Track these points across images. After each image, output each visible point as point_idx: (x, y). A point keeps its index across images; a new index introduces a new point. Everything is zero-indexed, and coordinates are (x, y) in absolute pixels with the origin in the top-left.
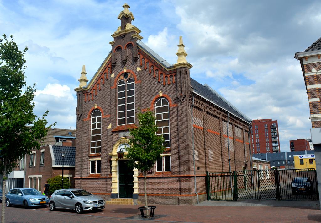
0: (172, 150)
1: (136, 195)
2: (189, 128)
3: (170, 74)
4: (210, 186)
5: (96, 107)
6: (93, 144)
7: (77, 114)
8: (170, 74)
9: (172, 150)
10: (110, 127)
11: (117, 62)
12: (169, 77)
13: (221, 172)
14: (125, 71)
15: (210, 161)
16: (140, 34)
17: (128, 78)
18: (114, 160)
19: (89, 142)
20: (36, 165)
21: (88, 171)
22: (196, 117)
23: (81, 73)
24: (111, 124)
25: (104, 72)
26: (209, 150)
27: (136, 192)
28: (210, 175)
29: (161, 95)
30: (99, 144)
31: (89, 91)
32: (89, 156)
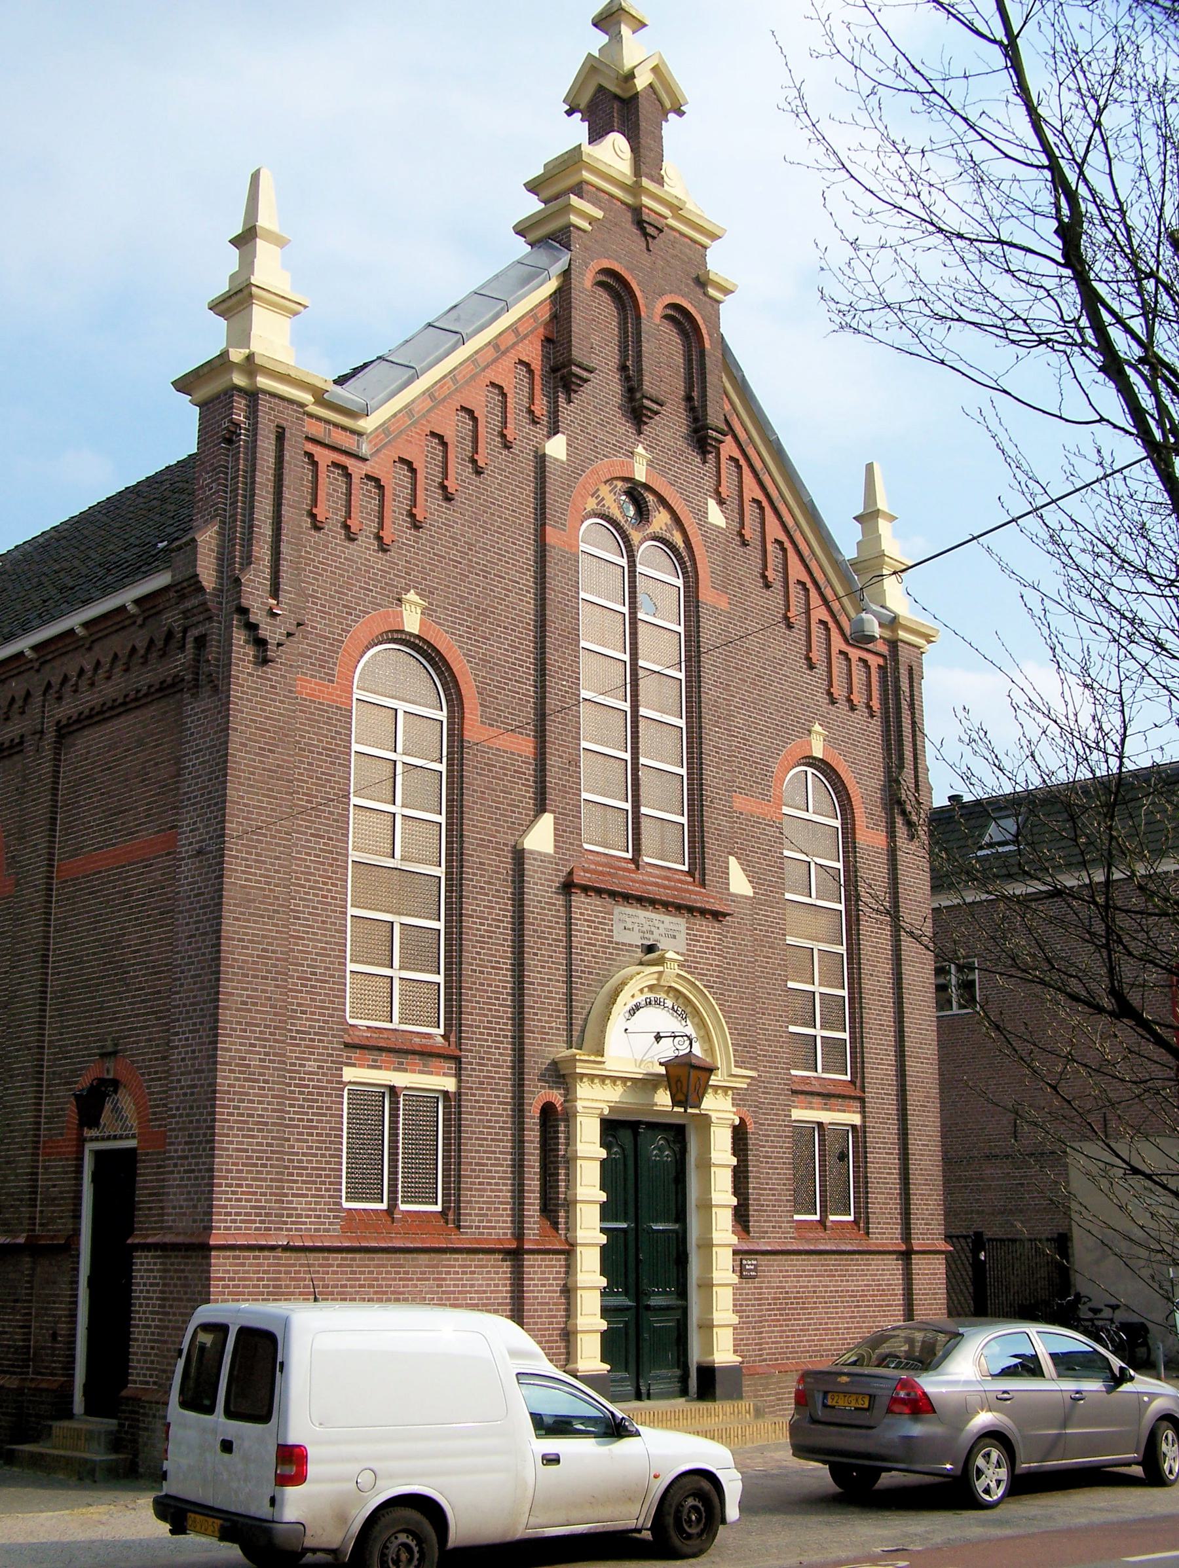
9: (869, 1096)
29: (412, 622)
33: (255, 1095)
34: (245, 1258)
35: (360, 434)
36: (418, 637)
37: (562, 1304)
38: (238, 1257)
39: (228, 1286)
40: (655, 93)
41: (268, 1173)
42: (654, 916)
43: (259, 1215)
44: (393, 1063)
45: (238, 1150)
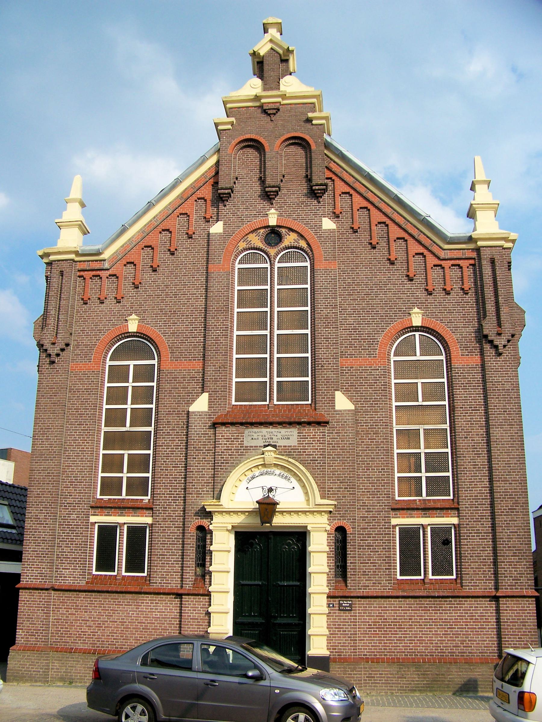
0: (464, 504)
1: (322, 663)
5: (133, 326)
6: (113, 464)
9: (462, 507)
11: (237, 187)
12: (447, 267)
14: (273, 221)
16: (222, 117)
17: (283, 245)
18: (221, 529)
19: (95, 452)
21: (84, 563)
25: (179, 210)
27: (317, 646)
29: (417, 320)
30: (140, 463)
31: (107, 266)
32: (93, 504)
33: (42, 529)
34: (34, 593)
35: (104, 260)
36: (137, 332)
37: (206, 619)
38: (31, 593)
39: (26, 604)
40: (275, 51)
41: (46, 560)
42: (274, 430)
43: (41, 576)
44: (118, 513)
45: (33, 551)
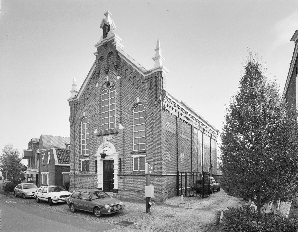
0: (147, 151)
2: (162, 131)
3: (146, 80)
4: (180, 184)
7: (70, 122)
8: (146, 80)
9: (146, 152)
10: (95, 132)
11: (101, 72)
13: (191, 172)
14: (107, 81)
15: (181, 162)
20: (47, 171)
22: (170, 122)
23: (72, 85)
24: (96, 129)
25: (90, 83)
26: (181, 153)
27: (116, 187)
28: (181, 174)
29: (138, 101)
31: (79, 101)
